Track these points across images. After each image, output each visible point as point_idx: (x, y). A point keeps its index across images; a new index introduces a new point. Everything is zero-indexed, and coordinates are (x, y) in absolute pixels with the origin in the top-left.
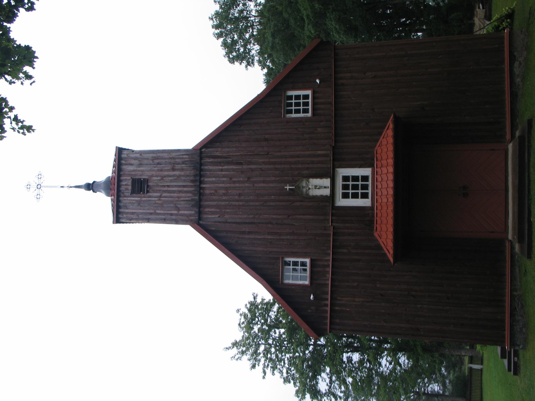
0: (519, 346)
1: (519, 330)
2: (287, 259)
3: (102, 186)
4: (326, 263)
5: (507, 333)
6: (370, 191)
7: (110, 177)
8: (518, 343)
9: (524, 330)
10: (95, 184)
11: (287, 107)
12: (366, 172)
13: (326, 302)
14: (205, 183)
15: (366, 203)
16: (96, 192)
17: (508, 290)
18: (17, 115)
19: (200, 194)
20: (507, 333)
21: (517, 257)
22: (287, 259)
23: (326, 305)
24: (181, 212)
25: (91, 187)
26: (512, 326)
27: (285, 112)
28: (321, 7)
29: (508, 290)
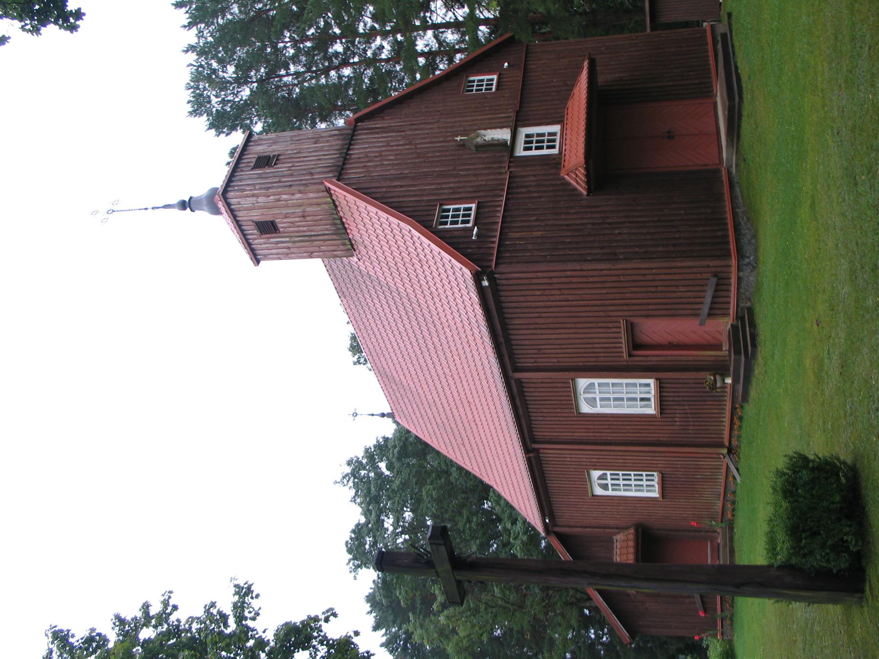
0: (749, 257)
1: (746, 242)
2: (472, 78)
3: (205, 202)
4: (499, 203)
5: (732, 247)
6: (557, 144)
7: (218, 189)
8: (748, 255)
9: (753, 241)
10: (192, 200)
11: (441, 219)
12: (556, 128)
13: (495, 227)
14: (353, 149)
15: (555, 151)
16: (194, 211)
17: (728, 209)
18: (173, 4)
19: (345, 159)
20: (732, 247)
21: (736, 180)
22: (472, 78)
23: (494, 242)
24: (314, 177)
25: (187, 205)
26: (738, 241)
27: (438, 223)
28: (422, 577)
29: (728, 209)
